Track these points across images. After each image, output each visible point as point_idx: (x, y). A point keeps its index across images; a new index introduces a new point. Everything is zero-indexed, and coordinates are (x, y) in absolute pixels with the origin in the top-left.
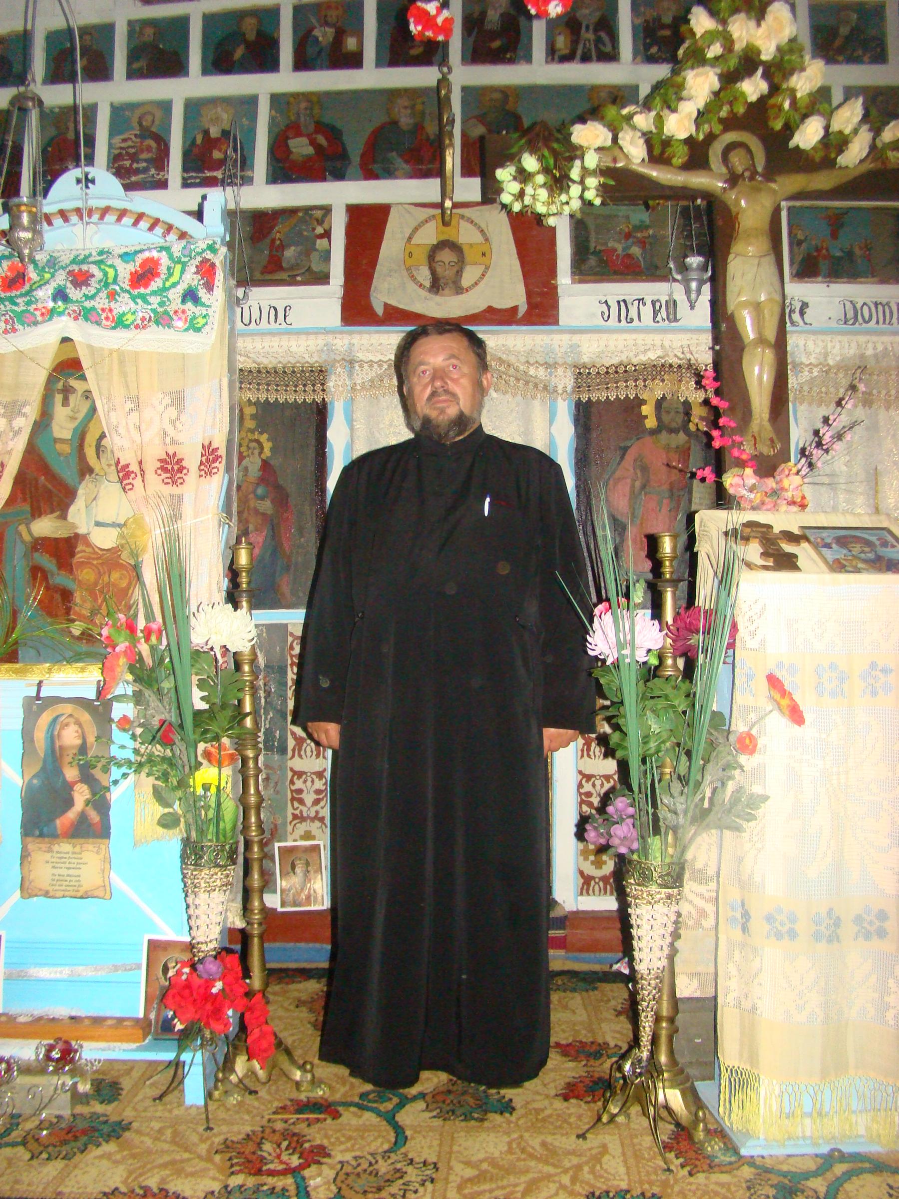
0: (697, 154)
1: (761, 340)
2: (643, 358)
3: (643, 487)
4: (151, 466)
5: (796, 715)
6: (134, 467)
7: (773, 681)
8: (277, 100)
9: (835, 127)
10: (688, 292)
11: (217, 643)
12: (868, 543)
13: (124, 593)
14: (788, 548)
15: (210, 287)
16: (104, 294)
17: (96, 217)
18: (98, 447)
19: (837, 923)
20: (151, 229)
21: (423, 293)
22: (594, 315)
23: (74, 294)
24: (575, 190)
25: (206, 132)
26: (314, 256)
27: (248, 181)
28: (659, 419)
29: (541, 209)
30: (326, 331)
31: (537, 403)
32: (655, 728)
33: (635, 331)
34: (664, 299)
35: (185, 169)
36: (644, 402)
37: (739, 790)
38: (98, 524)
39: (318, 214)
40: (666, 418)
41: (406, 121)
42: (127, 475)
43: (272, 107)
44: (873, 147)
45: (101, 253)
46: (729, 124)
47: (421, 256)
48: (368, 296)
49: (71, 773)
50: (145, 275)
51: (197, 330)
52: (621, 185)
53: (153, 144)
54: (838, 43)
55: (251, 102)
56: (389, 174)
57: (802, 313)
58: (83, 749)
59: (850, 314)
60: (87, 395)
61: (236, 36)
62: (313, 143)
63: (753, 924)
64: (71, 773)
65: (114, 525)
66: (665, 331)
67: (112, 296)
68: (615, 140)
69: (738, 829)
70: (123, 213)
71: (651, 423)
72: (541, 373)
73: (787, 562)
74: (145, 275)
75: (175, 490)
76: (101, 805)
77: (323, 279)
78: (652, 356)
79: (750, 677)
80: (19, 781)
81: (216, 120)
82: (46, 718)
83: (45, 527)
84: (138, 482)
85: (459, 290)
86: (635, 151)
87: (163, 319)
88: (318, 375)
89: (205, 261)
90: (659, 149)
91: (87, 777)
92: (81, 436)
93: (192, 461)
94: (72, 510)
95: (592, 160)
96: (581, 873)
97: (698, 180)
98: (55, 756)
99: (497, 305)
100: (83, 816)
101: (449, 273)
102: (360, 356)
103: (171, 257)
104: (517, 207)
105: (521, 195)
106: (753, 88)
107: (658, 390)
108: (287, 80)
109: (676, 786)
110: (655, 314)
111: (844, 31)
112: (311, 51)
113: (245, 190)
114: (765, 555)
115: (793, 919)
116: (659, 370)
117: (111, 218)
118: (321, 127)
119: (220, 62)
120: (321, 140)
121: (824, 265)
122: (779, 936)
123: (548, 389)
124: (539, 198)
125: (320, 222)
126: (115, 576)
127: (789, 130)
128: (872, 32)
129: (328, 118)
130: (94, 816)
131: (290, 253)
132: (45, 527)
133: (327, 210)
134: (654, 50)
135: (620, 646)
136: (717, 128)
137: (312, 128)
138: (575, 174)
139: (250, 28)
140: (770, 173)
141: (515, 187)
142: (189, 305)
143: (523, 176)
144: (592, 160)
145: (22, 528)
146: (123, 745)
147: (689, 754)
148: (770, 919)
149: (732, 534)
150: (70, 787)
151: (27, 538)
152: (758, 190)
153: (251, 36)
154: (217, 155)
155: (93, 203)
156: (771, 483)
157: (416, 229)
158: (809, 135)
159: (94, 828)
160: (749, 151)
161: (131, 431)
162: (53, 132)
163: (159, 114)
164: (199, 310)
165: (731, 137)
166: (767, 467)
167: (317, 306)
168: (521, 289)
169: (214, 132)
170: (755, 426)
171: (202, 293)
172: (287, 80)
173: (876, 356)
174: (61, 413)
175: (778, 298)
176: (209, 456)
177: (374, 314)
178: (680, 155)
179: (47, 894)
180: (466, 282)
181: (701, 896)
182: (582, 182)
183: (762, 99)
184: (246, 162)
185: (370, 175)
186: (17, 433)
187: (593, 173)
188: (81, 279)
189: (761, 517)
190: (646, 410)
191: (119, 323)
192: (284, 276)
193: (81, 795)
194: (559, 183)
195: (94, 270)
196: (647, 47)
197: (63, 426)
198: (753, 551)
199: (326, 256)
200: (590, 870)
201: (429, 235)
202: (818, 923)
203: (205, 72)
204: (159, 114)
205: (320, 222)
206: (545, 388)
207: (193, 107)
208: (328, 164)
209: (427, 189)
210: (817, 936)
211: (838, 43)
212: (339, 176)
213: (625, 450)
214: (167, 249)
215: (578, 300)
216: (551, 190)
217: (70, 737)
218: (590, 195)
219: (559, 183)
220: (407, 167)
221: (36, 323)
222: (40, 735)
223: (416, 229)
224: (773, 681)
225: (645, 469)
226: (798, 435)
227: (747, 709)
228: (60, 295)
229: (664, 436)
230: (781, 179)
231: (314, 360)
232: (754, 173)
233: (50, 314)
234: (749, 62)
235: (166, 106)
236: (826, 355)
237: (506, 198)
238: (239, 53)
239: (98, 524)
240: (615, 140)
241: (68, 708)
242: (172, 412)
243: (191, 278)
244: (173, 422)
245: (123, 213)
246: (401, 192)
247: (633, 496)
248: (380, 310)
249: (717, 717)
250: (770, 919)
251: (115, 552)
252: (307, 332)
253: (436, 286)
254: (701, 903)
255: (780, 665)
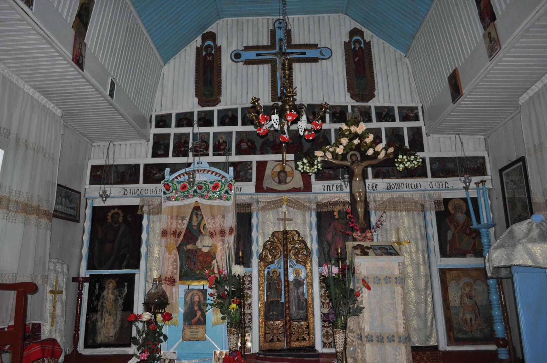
0: (344, 157)
1: (361, 200)
2: (334, 200)
3: (335, 234)
4: (218, 232)
5: (369, 288)
6: (214, 233)
7: (363, 280)
8: (237, 133)
9: (376, 150)
10: (345, 184)
11: (237, 274)
12: (386, 249)
13: (210, 263)
14: (366, 250)
15: (231, 190)
16: (206, 191)
17: (202, 172)
18: (204, 227)
19: (383, 338)
20: (216, 175)
21: (277, 184)
22: (320, 189)
23: (199, 191)
24: (316, 167)
25: (219, 141)
26: (248, 174)
27: (230, 154)
28: (339, 216)
29: (308, 171)
30: (251, 194)
31: (307, 213)
32: (338, 292)
33: (332, 193)
34: (339, 185)
35: (213, 151)
36: (335, 211)
37: (358, 306)
38: (204, 246)
39: (249, 163)
40: (341, 216)
41: (271, 139)
42: (212, 235)
43: (236, 135)
44: (386, 154)
45: (205, 181)
46: (351, 149)
47: (276, 174)
48: (262, 185)
49: (196, 308)
50: (216, 187)
51: (228, 200)
52: (326, 164)
53: (204, 143)
54: (383, 116)
55: (231, 133)
56: (267, 153)
57: (376, 187)
58: (199, 301)
59: (389, 187)
60: (201, 215)
61: (227, 116)
62: (247, 144)
63: (363, 339)
64: (196, 308)
65: (207, 246)
66: (339, 193)
67: (208, 192)
68: (325, 154)
69: (358, 315)
70: (209, 171)
71: (337, 217)
72: (308, 204)
73: (365, 254)
74: (216, 187)
75: (223, 238)
76: (204, 316)
77: (250, 180)
78: (336, 199)
79: (359, 280)
80: (183, 312)
81: (222, 138)
82: (190, 294)
83: (190, 247)
84: (214, 236)
85: (286, 183)
86: (329, 156)
87: (220, 198)
88: (249, 205)
89: (230, 184)
90: (335, 155)
91: (200, 309)
92: (199, 224)
93: (227, 231)
94: (197, 243)
95: (319, 159)
96: (323, 342)
97: (344, 163)
98: (192, 303)
99: (296, 187)
100: (199, 319)
101: (283, 179)
102: (260, 200)
103: (222, 183)
104: (302, 171)
105: (303, 168)
106: (356, 141)
107: (338, 208)
108: (240, 128)
109: (343, 306)
110: (337, 188)
111: (384, 113)
112: (246, 120)
113: (230, 157)
114: (361, 252)
115: (372, 337)
116: (338, 203)
117: (206, 172)
118: (249, 140)
119: (222, 123)
120: (249, 144)
121: (381, 175)
122: (369, 341)
123: (310, 209)
124: (307, 169)
125: (249, 165)
126: (208, 259)
127: (366, 151)
128: (391, 114)
129: (251, 138)
130: (202, 319)
131: (241, 173)
132: (190, 247)
133: (251, 162)
134: (335, 119)
135: (329, 273)
136: (349, 151)
137: (247, 141)
138: (316, 163)
139: (230, 114)
140: (362, 161)
141: (302, 166)
142: (226, 194)
143: (304, 164)
144: (319, 159)
145: (185, 247)
146: (210, 300)
147: (346, 298)
148: (367, 337)
149: (355, 248)
150: (196, 312)
151: (185, 249)
152: (359, 165)
153: (230, 116)
154: (222, 147)
155: (201, 169)
156: (364, 235)
157: (274, 167)
158: (370, 152)
159: (202, 322)
160: (357, 157)
161: (210, 224)
162: (177, 140)
163: (206, 136)
164: (229, 196)
165: (352, 153)
166: (363, 231)
167: (249, 188)
168: (302, 183)
169: (221, 141)
170: (360, 221)
171: (229, 191)
172: (240, 128)
173: (397, 198)
174: (194, 218)
175: (364, 190)
176: (231, 230)
177: (264, 189)
178: (340, 157)
179: (189, 340)
180: (287, 181)
181: (352, 336)
182: (317, 165)
183: (359, 144)
184: (230, 149)
185: (262, 153)
186: (184, 224)
187: (320, 163)
188: (200, 188)
189: (361, 243)
190: (335, 213)
191: (210, 198)
192: (240, 179)
193: (199, 314)
194: (312, 165)
195: (203, 186)
196: (333, 119)
197: (195, 223)
198: (358, 251)
199: (251, 174)
200: (326, 341)
201: (278, 169)
202: (378, 338)
203: (218, 125)
204: (206, 136)
205: (249, 165)
206: (309, 208)
207: (215, 134)
208: (251, 151)
209: (279, 157)
210: (378, 341)
211: (383, 116)
212: (254, 154)
213: (330, 224)
214: (221, 181)
215: (317, 186)
216: (310, 168)
217: (196, 299)
218: (319, 167)
219: (312, 165)
220: (272, 151)
221: (189, 198)
222: (188, 299)
223: (274, 167)
224: (363, 280)
225: (335, 229)
226: (374, 220)
227: (358, 287)
228: (195, 191)
229: (340, 221)
230: (364, 162)
231: (249, 201)
232: (358, 161)
233: (193, 196)
234: (356, 135)
235: (208, 134)
236: (383, 198)
237: (300, 169)
238: (227, 120)
239: (204, 246)
240: (325, 154)
241: (196, 292)
242: (223, 219)
243: (226, 188)
244: (223, 222)
245: (209, 171)
246: (271, 158)
247: (333, 237)
248: (265, 188)
249: (352, 291)
250: (367, 337)
251: (208, 253)
252: (246, 194)
253: (280, 182)
254: (352, 338)
255: (365, 277)
